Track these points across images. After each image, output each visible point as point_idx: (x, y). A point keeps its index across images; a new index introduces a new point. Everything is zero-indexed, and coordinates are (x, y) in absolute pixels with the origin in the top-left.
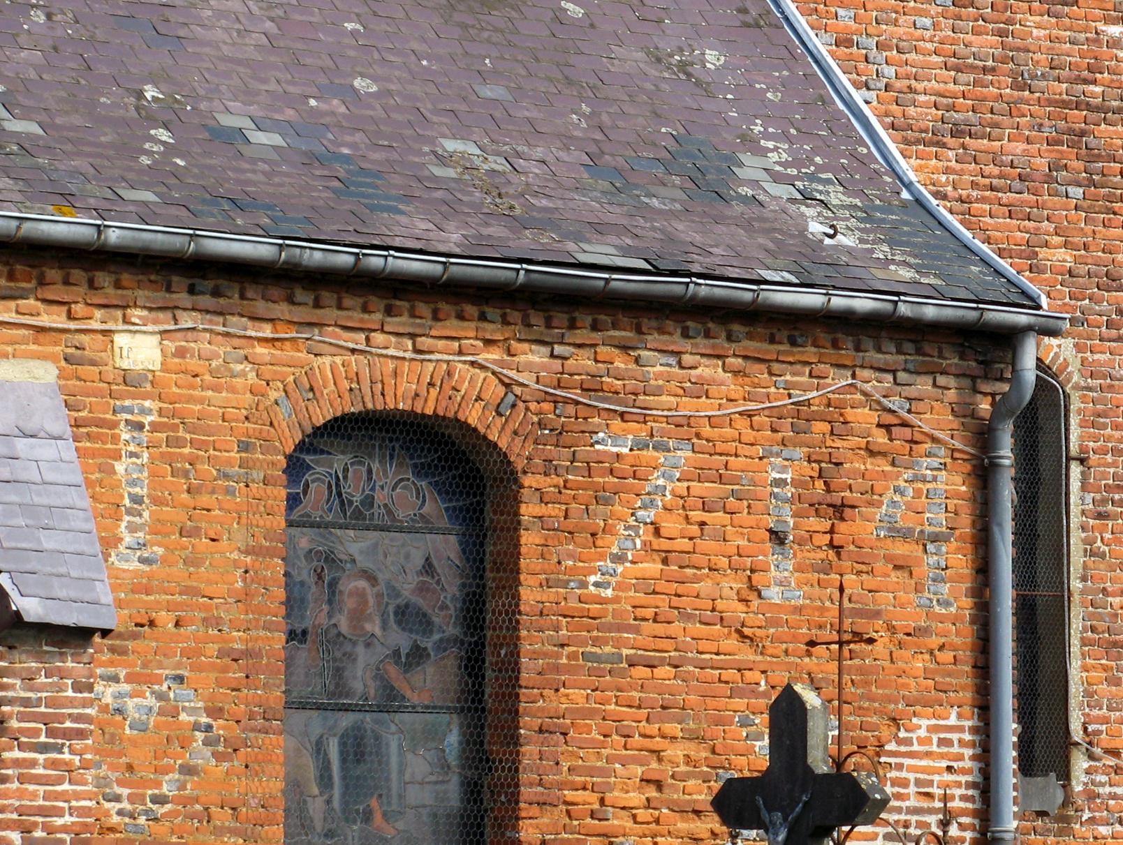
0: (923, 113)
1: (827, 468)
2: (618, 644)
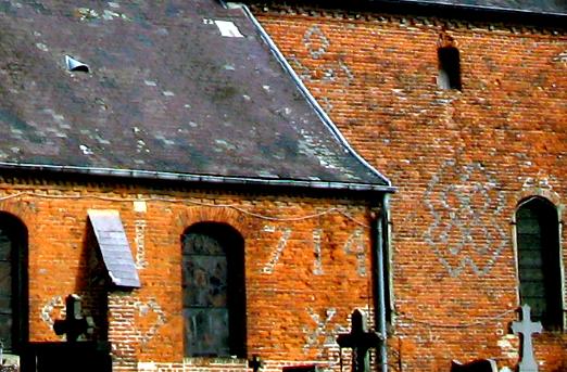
0: (342, 119)
1: (329, 234)
2: (273, 287)
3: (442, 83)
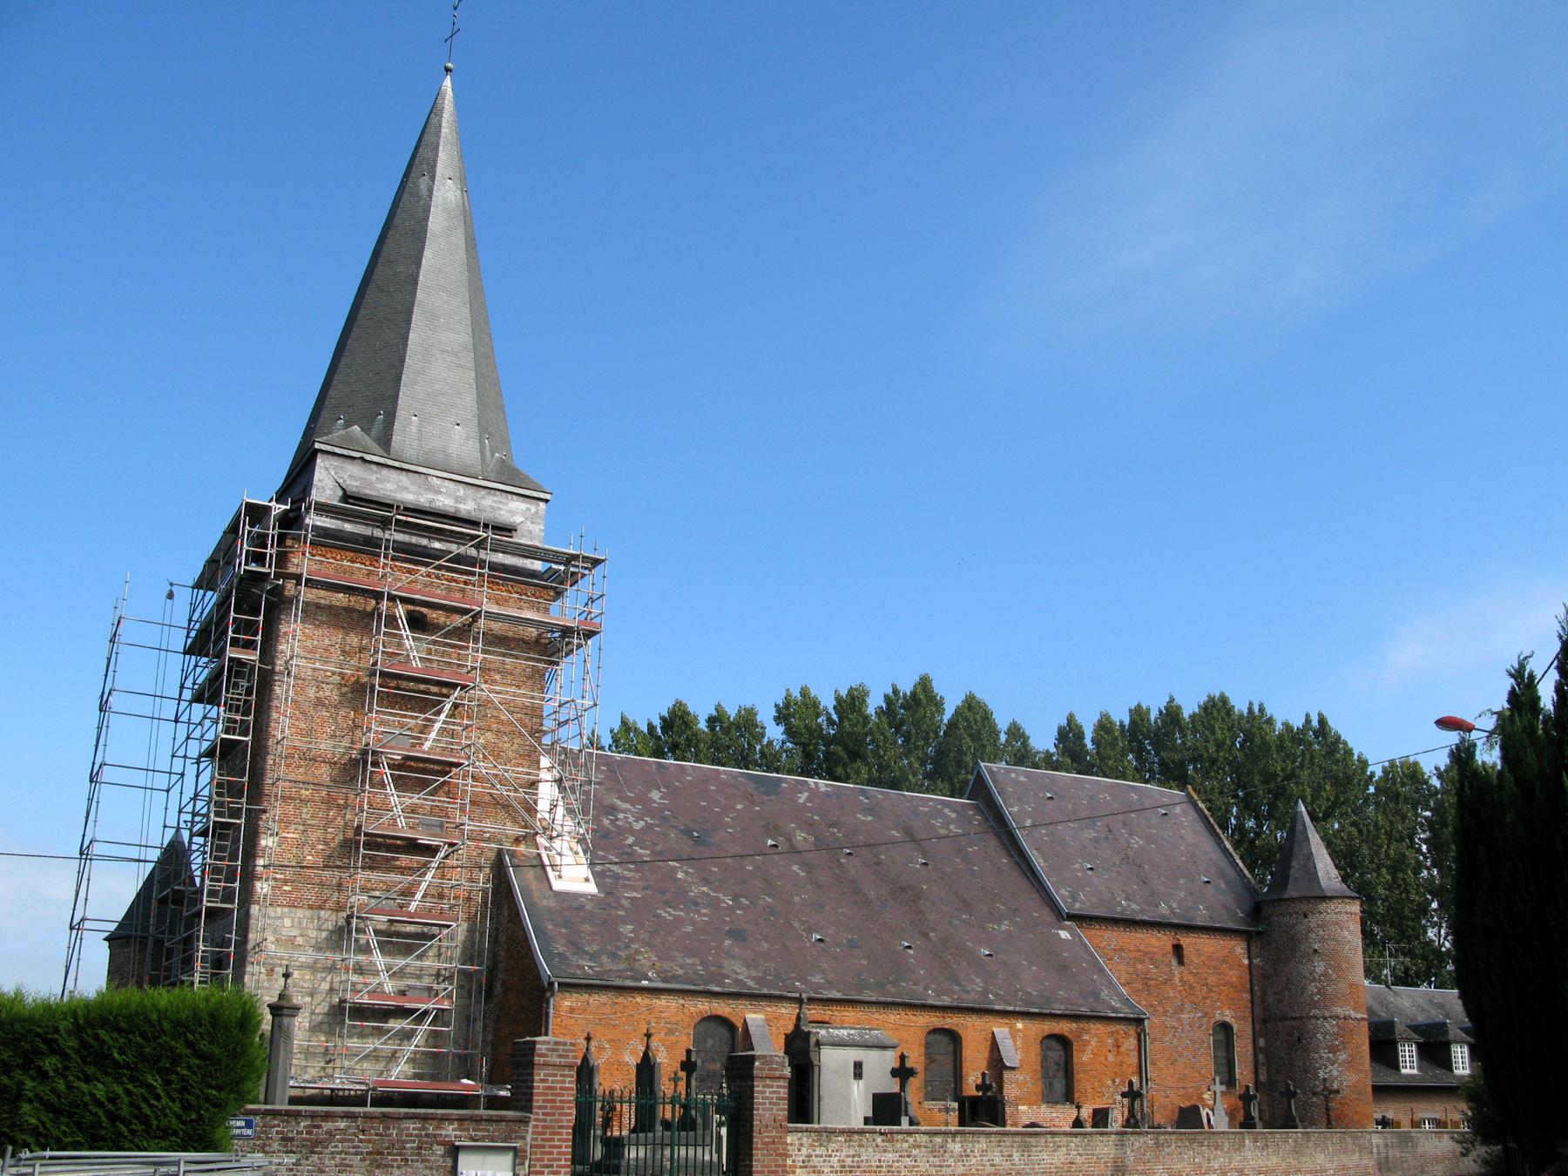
1: (1117, 1041)
3: (1174, 962)
